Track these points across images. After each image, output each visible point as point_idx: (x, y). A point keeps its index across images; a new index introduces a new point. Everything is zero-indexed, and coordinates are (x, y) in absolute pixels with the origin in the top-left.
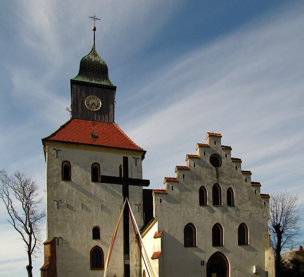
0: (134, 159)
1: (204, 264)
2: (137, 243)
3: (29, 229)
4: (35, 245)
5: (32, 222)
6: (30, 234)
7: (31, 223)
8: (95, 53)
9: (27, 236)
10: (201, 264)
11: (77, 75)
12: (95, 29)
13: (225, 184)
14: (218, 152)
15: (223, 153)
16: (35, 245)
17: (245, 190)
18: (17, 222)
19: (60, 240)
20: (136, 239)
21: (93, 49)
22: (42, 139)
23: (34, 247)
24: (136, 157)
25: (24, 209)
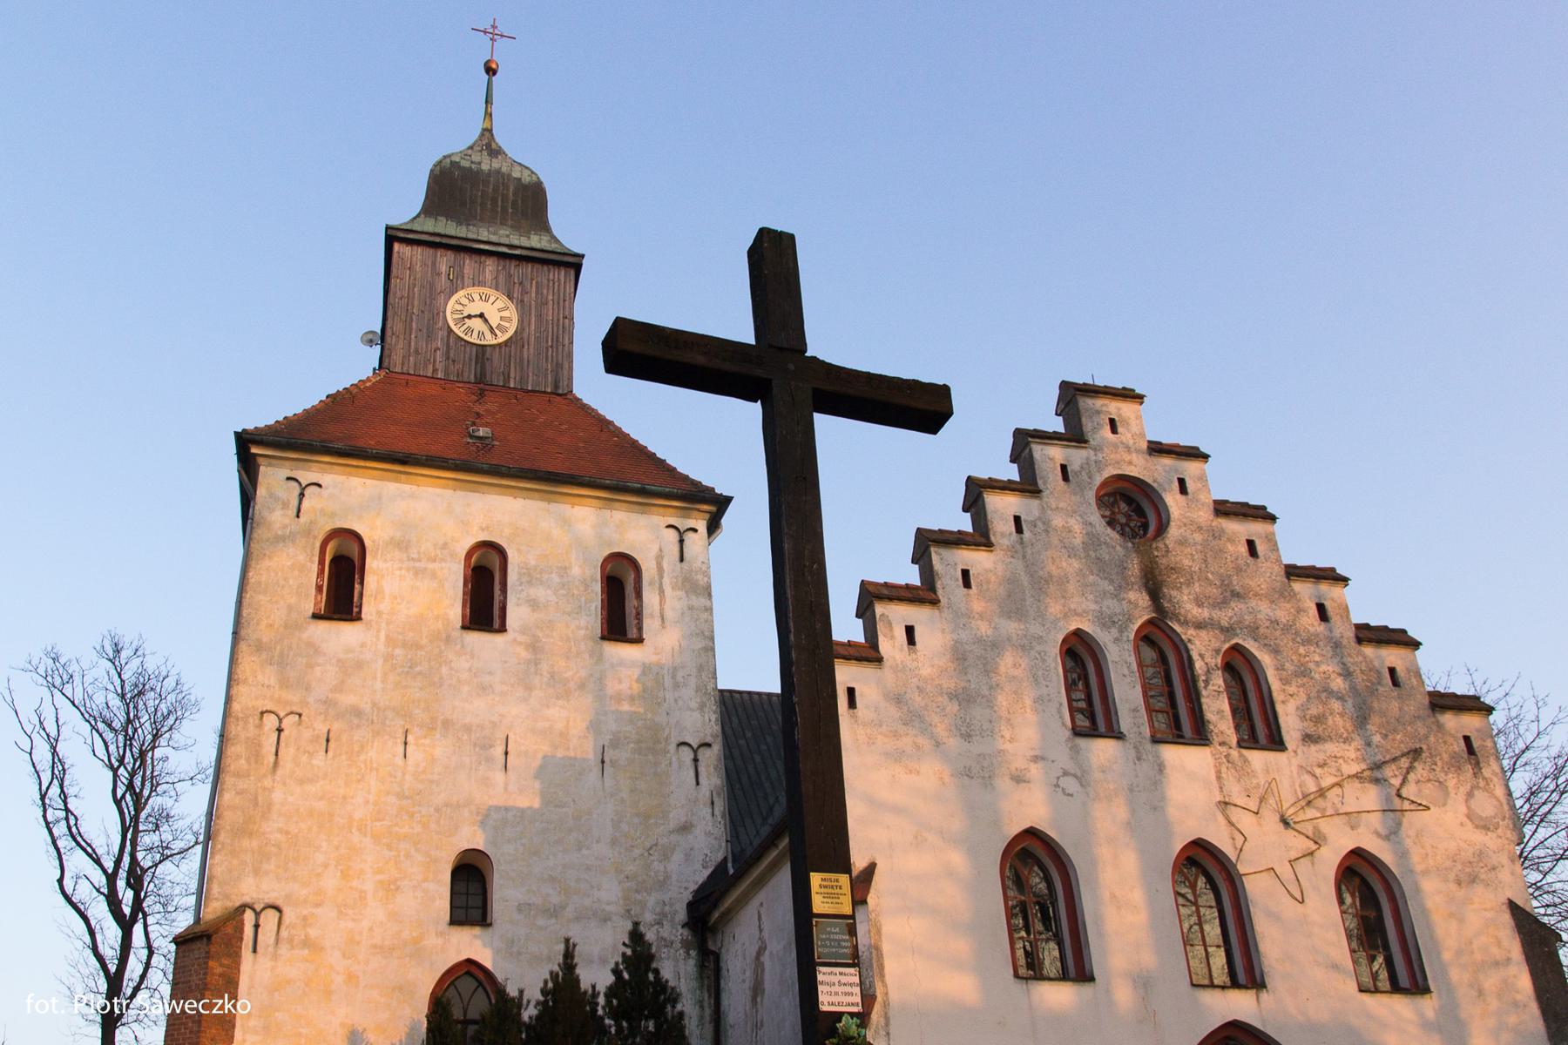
0: (672, 531)
2: (693, 953)
3: (127, 896)
4: (143, 977)
5: (146, 863)
6: (126, 925)
7: (144, 871)
8: (494, 146)
9: (110, 934)
11: (415, 214)
13: (1199, 626)
14: (1155, 658)
16: (143, 977)
18: (77, 861)
19: (270, 918)
20: (686, 932)
21: (487, 132)
22: (235, 432)
23: (137, 989)
24: (684, 524)
25: (118, 802)
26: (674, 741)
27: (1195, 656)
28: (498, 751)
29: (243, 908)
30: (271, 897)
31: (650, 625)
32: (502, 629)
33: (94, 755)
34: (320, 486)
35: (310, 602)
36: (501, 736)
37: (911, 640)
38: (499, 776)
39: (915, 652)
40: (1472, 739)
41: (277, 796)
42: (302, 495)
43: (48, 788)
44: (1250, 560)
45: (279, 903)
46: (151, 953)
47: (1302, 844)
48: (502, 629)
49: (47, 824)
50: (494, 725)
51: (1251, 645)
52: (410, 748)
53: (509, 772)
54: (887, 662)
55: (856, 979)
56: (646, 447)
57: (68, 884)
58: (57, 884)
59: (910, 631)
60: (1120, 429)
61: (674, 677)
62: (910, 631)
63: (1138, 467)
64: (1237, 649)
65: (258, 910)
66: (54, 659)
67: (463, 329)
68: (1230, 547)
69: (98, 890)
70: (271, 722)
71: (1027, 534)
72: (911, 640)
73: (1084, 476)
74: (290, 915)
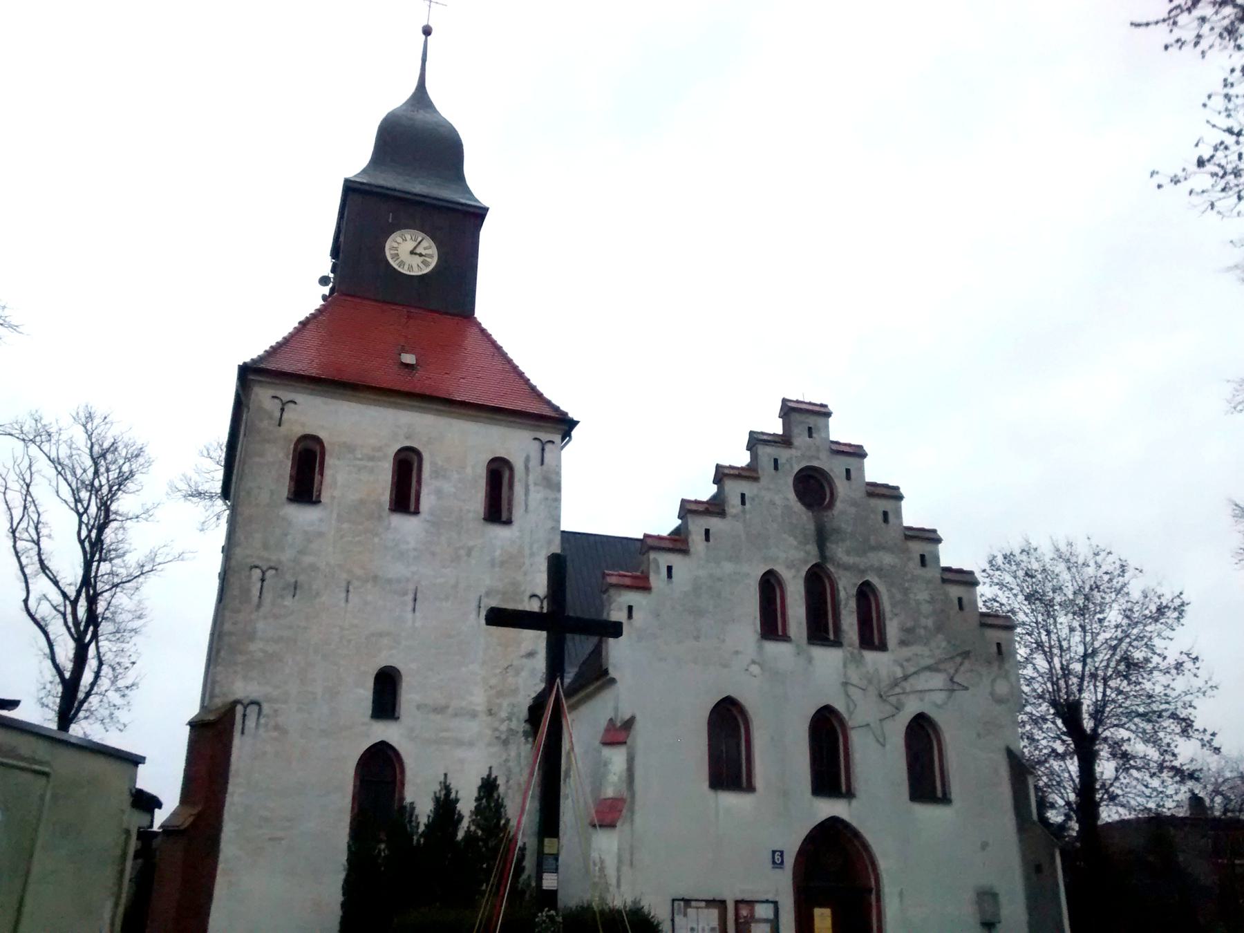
0: (537, 444)
1: (782, 862)
10: (774, 862)
12: (427, 31)
13: (846, 568)
15: (835, 467)
16: (93, 684)
17: (921, 595)
18: (41, 585)
19: (252, 710)
25: (82, 542)
26: (528, 594)
27: (841, 588)
28: (410, 597)
29: (236, 703)
30: (254, 696)
31: (518, 513)
32: (417, 512)
33: (58, 496)
34: (295, 403)
35: (284, 488)
36: (411, 587)
37: (670, 575)
38: (409, 615)
39: (672, 583)
40: (1002, 645)
41: (260, 625)
42: (283, 410)
43: (19, 524)
44: (883, 525)
45: (260, 699)
46: (101, 663)
47: (888, 709)
48: (417, 512)
49: (17, 553)
50: (408, 580)
51: (875, 581)
52: (351, 595)
53: (417, 613)
54: (654, 590)
55: (556, 878)
56: (524, 373)
57: (32, 604)
58: (22, 604)
59: (670, 569)
60: (814, 435)
61: (531, 548)
62: (670, 569)
63: (824, 462)
64: (867, 584)
65: (245, 705)
66: (36, 421)
67: (397, 262)
68: (872, 516)
69: (55, 608)
70: (257, 573)
71: (748, 505)
72: (670, 575)
73: (788, 466)
74: (266, 708)
